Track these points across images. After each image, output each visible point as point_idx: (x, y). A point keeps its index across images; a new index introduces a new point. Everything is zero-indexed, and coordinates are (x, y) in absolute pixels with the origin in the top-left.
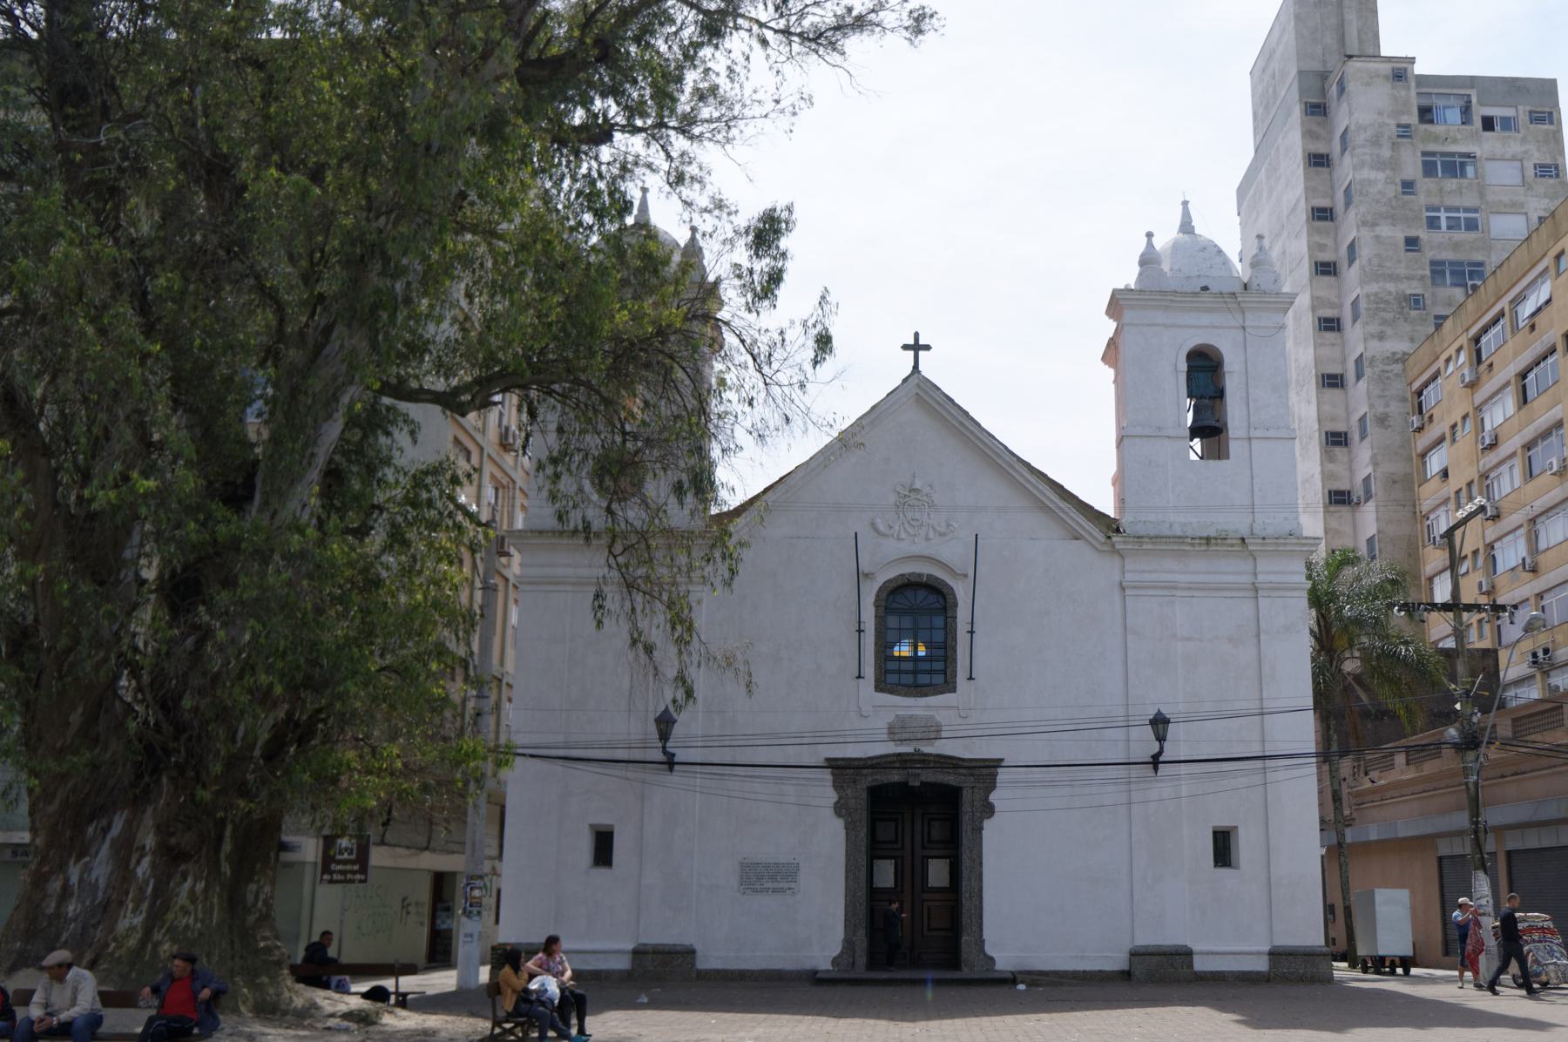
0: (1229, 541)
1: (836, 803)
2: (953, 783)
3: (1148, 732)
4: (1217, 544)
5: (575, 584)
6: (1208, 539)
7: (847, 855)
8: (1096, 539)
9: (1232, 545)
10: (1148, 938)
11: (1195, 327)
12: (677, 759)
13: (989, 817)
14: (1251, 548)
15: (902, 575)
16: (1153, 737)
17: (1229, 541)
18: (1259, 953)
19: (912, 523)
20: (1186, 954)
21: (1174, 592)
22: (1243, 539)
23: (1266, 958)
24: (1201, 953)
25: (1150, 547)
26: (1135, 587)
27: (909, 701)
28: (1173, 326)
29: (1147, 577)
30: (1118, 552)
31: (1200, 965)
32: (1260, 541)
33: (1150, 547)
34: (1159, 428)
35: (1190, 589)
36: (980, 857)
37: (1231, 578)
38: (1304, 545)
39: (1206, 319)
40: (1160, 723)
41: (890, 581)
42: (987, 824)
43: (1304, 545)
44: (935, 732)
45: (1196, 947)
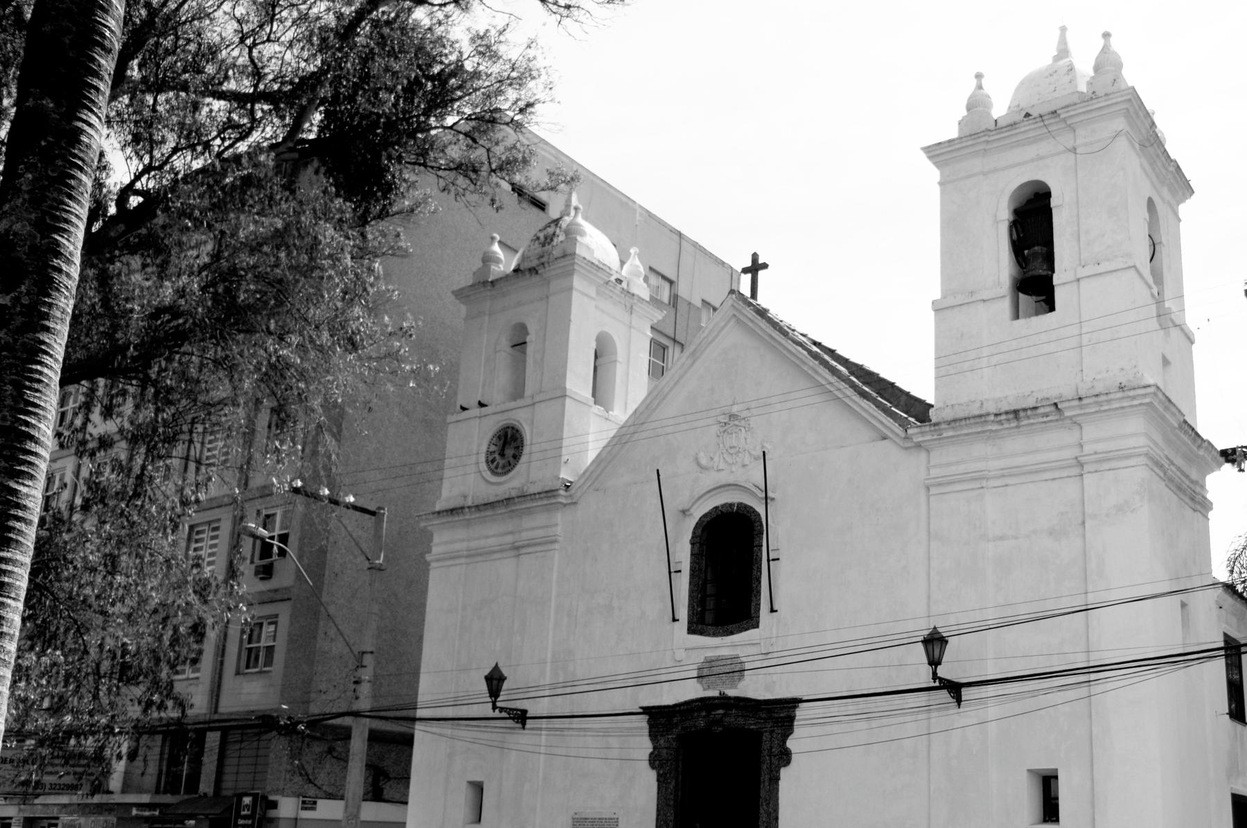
1: (651, 754)
4: (1028, 417)
5: (467, 556)
7: (658, 810)
8: (897, 435)
11: (1019, 164)
13: (784, 766)
14: (1067, 414)
15: (716, 508)
17: (1041, 411)
21: (984, 483)
22: (1056, 404)
25: (951, 433)
26: (940, 484)
28: (995, 170)
29: (953, 470)
33: (951, 433)
36: (776, 810)
37: (1053, 456)
38: (1134, 398)
39: (1031, 151)
40: (935, 643)
41: (705, 516)
42: (784, 773)
43: (1134, 398)
44: (737, 671)
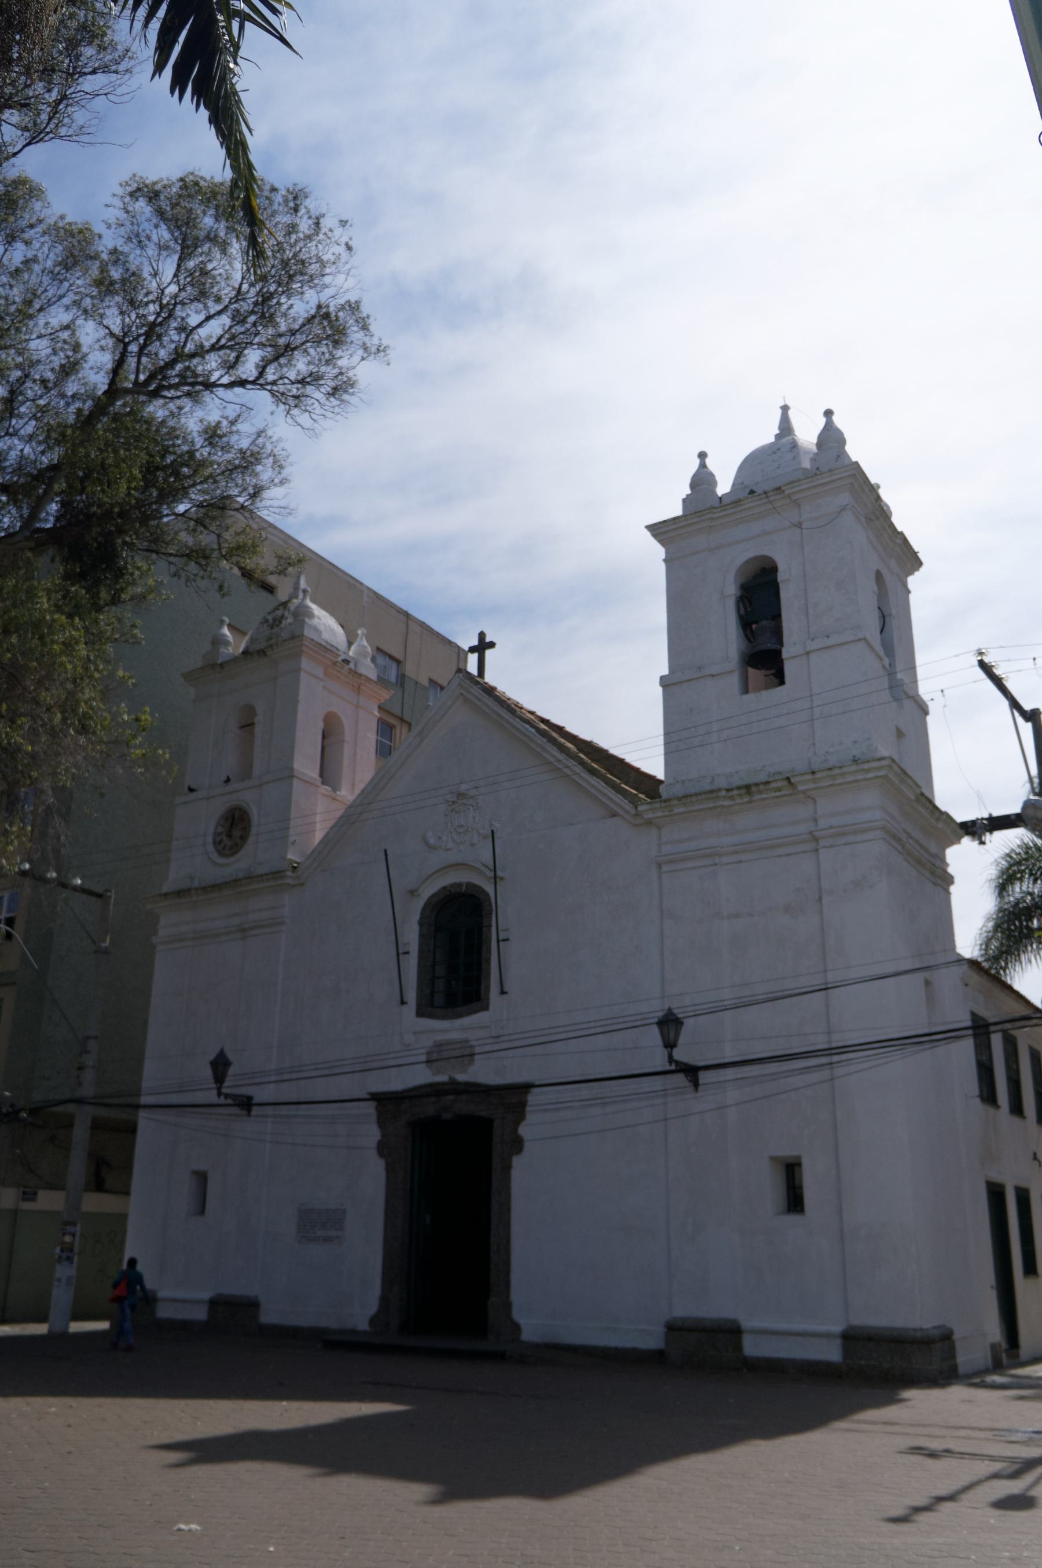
0: (774, 785)
1: (379, 1143)
2: (484, 1114)
3: (654, 1036)
4: (760, 792)
6: (748, 788)
9: (779, 789)
10: (685, 1308)
12: (254, 1102)
14: (801, 788)
16: (659, 1041)
17: (774, 785)
18: (828, 1335)
19: (460, 830)
20: (733, 1331)
21: (717, 860)
22: (788, 779)
23: (838, 1342)
24: (754, 1332)
25: (682, 810)
26: (671, 862)
27: (445, 1024)
30: (649, 823)
31: (751, 1347)
32: (809, 777)
33: (682, 810)
34: (700, 668)
35: (736, 852)
38: (868, 771)
41: (433, 896)
43: (868, 771)
45: (747, 1323)
